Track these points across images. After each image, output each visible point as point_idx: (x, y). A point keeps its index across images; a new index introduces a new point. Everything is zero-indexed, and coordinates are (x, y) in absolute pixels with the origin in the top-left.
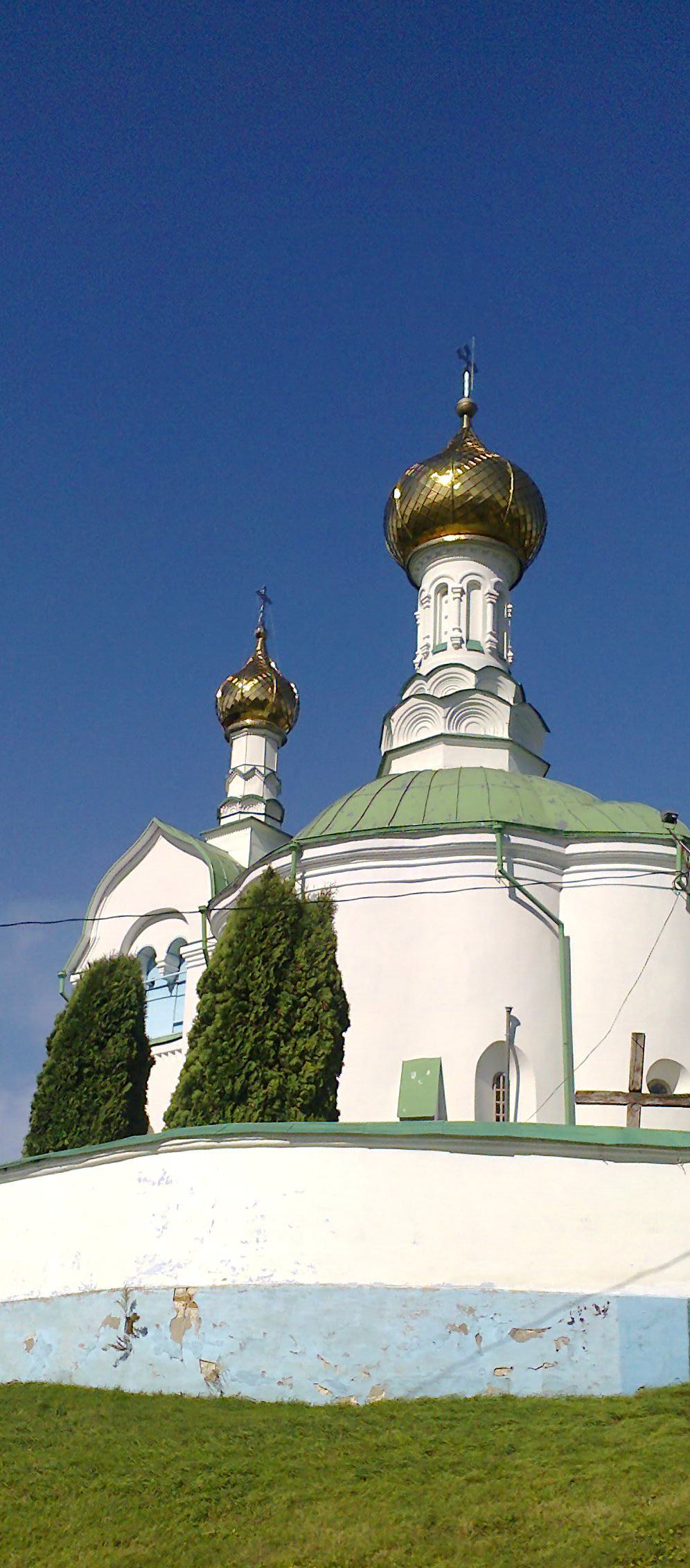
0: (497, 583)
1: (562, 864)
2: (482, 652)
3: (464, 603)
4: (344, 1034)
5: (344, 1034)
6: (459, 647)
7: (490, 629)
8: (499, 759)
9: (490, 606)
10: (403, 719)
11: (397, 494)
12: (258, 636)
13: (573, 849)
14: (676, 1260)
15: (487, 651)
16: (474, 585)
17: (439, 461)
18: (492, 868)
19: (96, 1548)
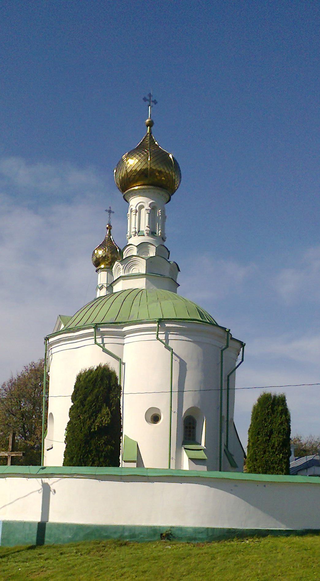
0: (150, 204)
1: (123, 335)
2: (144, 235)
3: (137, 217)
4: (72, 404)
5: (72, 404)
6: (135, 236)
7: (147, 225)
8: (141, 284)
9: (147, 214)
10: (115, 270)
11: (115, 171)
12: (107, 228)
13: (126, 329)
14: (29, 494)
15: (146, 234)
16: (142, 207)
17: (131, 154)
18: (93, 341)
19: (274, 576)
